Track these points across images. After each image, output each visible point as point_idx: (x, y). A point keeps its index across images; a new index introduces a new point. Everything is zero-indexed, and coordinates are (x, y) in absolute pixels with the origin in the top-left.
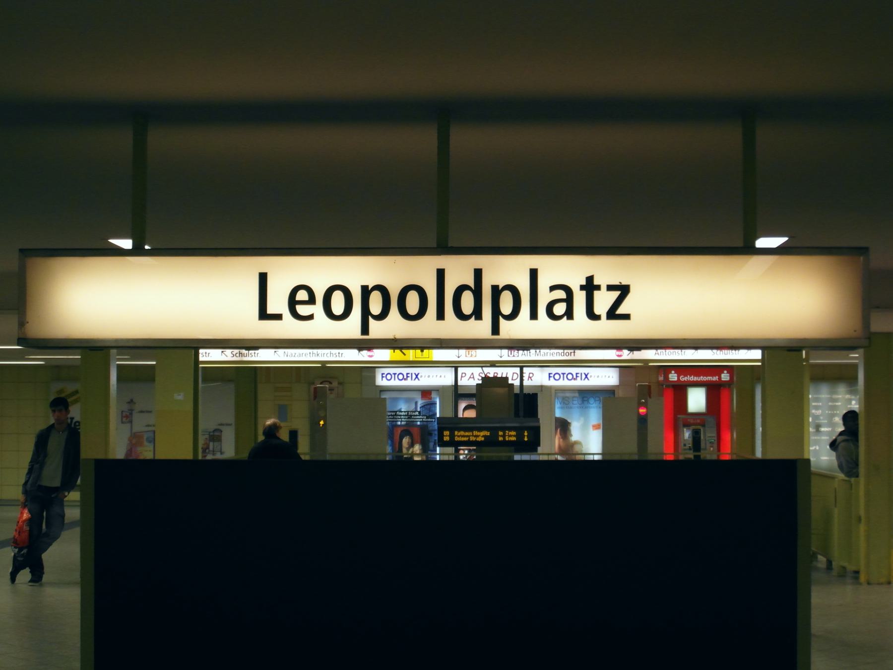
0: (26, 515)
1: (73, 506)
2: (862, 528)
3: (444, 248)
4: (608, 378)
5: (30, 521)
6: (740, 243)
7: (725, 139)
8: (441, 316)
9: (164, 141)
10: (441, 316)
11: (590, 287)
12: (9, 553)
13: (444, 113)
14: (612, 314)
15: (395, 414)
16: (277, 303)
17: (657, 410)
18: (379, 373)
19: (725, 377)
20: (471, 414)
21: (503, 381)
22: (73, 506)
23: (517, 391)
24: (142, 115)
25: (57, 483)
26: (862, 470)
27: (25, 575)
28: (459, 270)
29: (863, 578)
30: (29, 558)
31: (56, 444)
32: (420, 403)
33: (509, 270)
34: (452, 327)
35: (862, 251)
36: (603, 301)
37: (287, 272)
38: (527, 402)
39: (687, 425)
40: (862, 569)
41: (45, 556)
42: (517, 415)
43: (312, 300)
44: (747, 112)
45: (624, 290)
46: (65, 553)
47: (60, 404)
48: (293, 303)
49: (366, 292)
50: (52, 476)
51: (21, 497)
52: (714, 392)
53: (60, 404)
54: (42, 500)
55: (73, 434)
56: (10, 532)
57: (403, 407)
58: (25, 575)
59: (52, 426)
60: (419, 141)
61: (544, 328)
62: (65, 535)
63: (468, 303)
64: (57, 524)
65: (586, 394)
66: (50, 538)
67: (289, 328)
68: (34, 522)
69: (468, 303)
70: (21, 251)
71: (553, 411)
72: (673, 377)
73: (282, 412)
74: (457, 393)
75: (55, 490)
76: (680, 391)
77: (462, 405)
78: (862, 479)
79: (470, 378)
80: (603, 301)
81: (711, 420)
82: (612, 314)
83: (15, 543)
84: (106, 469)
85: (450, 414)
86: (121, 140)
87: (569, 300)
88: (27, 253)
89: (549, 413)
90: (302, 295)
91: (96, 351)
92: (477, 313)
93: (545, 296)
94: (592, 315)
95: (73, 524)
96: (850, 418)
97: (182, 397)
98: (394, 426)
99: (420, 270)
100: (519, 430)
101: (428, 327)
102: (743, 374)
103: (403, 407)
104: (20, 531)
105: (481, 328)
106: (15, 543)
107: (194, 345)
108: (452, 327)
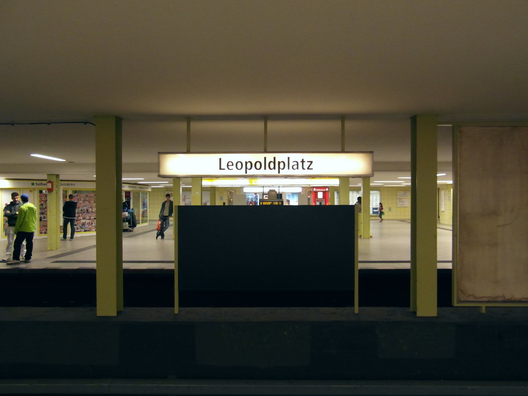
0: (160, 223)
1: (172, 220)
2: (362, 225)
3: (266, 152)
4: (300, 190)
5: (161, 224)
6: (340, 150)
7: (336, 125)
8: (265, 169)
9: (195, 126)
10: (265, 169)
11: (303, 161)
12: (156, 232)
13: (265, 118)
14: (308, 168)
15: (248, 199)
16: (224, 166)
17: (311, 197)
18: (244, 189)
19: (327, 189)
20: (267, 198)
21: (274, 191)
22: (172, 220)
23: (278, 193)
24: (189, 118)
25: (167, 215)
26: (362, 211)
27: (160, 237)
28: (270, 157)
29: (362, 237)
30: (161, 233)
31: (167, 206)
32: (254, 196)
33: (281, 157)
34: (268, 172)
35: (372, 152)
36: (306, 165)
37: (226, 158)
38: (280, 196)
39: (318, 201)
40: (362, 235)
41: (164, 233)
42: (278, 198)
43: (233, 165)
44: (342, 117)
45: (311, 162)
46: (170, 232)
47: (168, 196)
48: (228, 165)
49: (246, 163)
50: (166, 213)
51: (158, 218)
52: (325, 193)
53: (168, 196)
54: (164, 219)
55: (171, 203)
56: (156, 227)
57: (250, 197)
58: (160, 237)
59: (166, 201)
60: (259, 126)
61: (291, 172)
62: (169, 228)
63: (272, 165)
64: (168, 225)
65: (293, 194)
66: (166, 228)
67: (227, 172)
68: (162, 224)
69: (272, 165)
70: (159, 153)
71: (286, 197)
72: (315, 190)
73: (221, 198)
74: (264, 194)
75: (167, 216)
76: (316, 193)
77: (265, 196)
78: (362, 213)
79: (267, 190)
80: (306, 165)
81: (324, 200)
82: (308, 168)
83: (157, 229)
84: (180, 207)
85: (261, 198)
86: (183, 126)
87: (298, 165)
88: (160, 153)
89: (285, 198)
90: (230, 164)
91: (177, 179)
92: (274, 168)
93: (291, 164)
94: (303, 168)
95: (172, 225)
96: (359, 199)
97: (198, 193)
98: (248, 202)
99: (259, 157)
100: (279, 202)
101: (262, 172)
102: (333, 189)
103: (250, 197)
104: (159, 227)
105: (275, 172)
106: (157, 229)
107: (201, 177)
108: (268, 172)
